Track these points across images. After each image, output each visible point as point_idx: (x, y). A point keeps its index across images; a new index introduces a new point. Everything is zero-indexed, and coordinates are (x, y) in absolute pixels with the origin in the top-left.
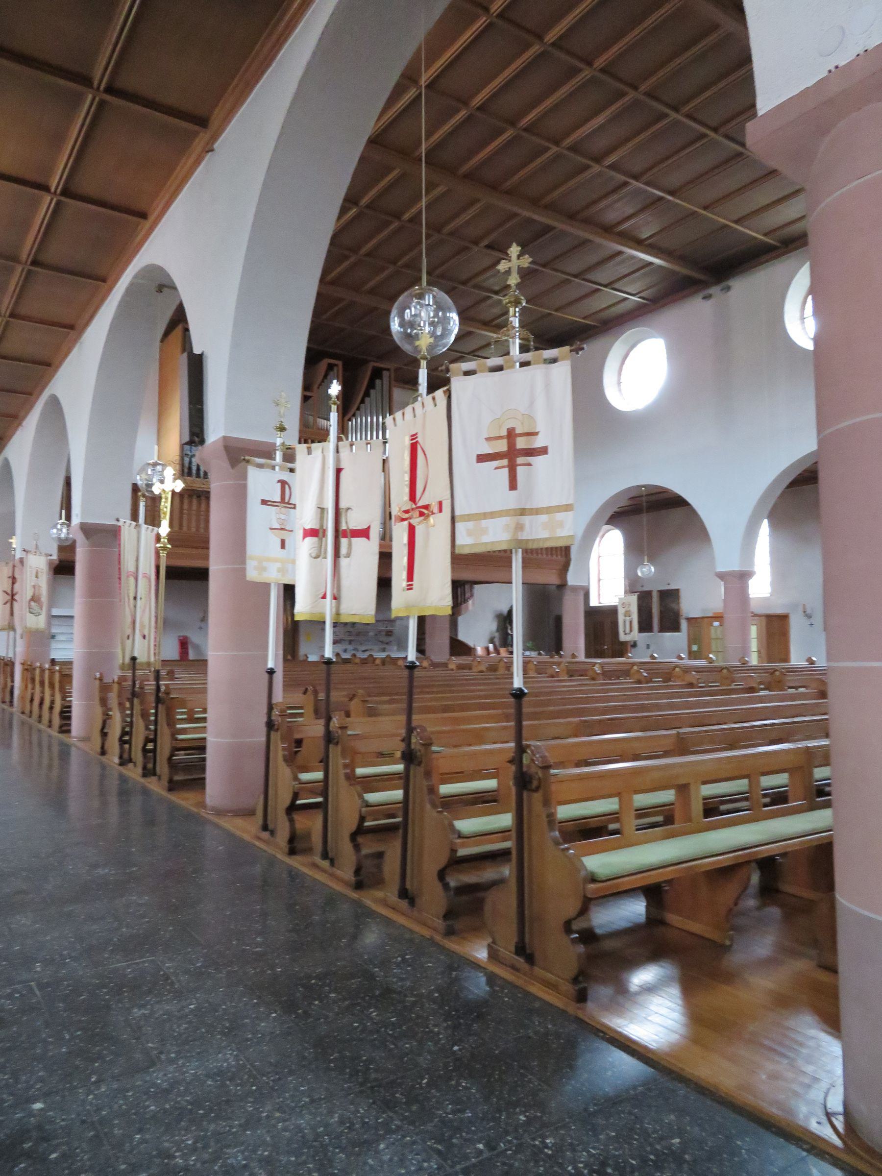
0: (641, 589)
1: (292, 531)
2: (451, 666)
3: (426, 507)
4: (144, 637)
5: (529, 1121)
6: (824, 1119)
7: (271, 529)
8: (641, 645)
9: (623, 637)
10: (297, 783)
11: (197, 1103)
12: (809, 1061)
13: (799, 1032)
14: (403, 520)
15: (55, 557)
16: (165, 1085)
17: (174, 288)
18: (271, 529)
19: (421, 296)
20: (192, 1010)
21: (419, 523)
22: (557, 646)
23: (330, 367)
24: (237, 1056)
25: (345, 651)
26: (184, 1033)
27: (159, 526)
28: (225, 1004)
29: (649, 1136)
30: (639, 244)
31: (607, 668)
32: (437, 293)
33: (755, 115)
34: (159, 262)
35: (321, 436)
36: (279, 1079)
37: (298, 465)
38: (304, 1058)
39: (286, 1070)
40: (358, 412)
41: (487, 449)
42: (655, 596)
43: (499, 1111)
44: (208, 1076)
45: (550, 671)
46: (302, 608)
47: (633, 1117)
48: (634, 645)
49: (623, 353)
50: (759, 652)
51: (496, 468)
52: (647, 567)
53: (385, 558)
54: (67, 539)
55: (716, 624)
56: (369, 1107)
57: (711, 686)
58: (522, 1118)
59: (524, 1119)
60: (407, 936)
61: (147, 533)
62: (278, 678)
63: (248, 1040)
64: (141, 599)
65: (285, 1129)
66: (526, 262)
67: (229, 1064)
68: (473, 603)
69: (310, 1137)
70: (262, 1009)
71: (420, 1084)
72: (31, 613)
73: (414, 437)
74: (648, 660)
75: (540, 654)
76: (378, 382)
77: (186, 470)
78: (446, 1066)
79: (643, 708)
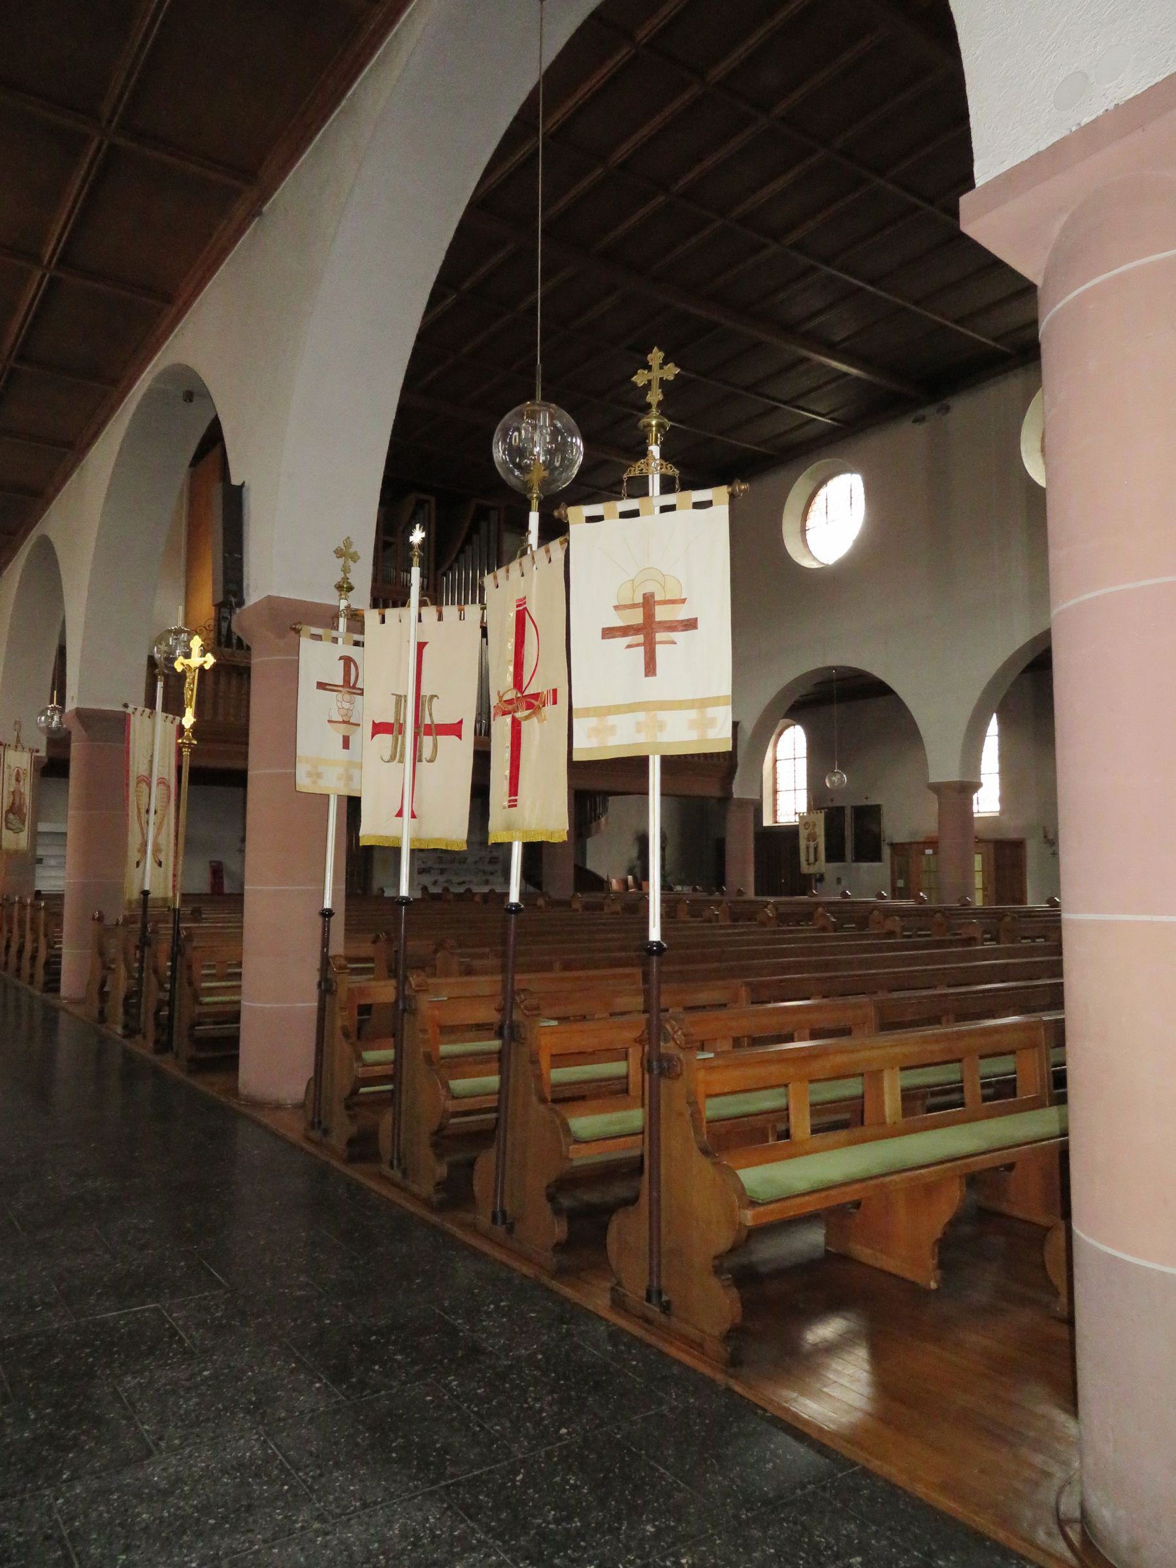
0: (830, 804)
1: (359, 725)
2: (576, 905)
3: (536, 696)
4: (160, 864)
5: (659, 1532)
6: (1055, 1529)
7: (329, 721)
8: (830, 878)
9: (805, 869)
10: (361, 1064)
11: (206, 1509)
12: (1038, 1446)
13: (1023, 1408)
14: (504, 713)
15: (43, 753)
16: (164, 1485)
17: (207, 395)
18: (329, 721)
19: (533, 415)
20: (207, 1378)
21: (527, 718)
22: (719, 880)
23: (420, 504)
24: (265, 1441)
25: (435, 883)
26: (194, 1411)
27: (182, 714)
28: (251, 1368)
29: (821, 1553)
30: (832, 349)
31: (782, 909)
32: (555, 411)
33: (972, 186)
34: (190, 362)
35: (402, 601)
36: (321, 1475)
37: (367, 638)
38: (357, 1445)
39: (331, 1463)
40: (456, 566)
41: (616, 621)
42: (848, 813)
43: (619, 1519)
44: (224, 1472)
45: (706, 914)
46: (371, 830)
47: (799, 1528)
48: (821, 878)
49: (810, 491)
50: (984, 889)
51: (629, 646)
52: (838, 776)
53: (482, 759)
54: (59, 729)
55: (929, 852)
56: (443, 1514)
57: (920, 936)
58: (650, 1528)
59: (653, 1530)
60: (503, 1275)
61: (162, 724)
62: (338, 924)
63: (280, 1420)
64: (156, 812)
65: (325, 1546)
66: (671, 372)
67: (253, 1453)
68: (607, 820)
69: (359, 1557)
70: (302, 1377)
71: (513, 1481)
72: (8, 828)
73: (521, 602)
74: (838, 898)
75: (695, 890)
76: (483, 525)
77: (223, 639)
78: (549, 1455)
79: (827, 966)
